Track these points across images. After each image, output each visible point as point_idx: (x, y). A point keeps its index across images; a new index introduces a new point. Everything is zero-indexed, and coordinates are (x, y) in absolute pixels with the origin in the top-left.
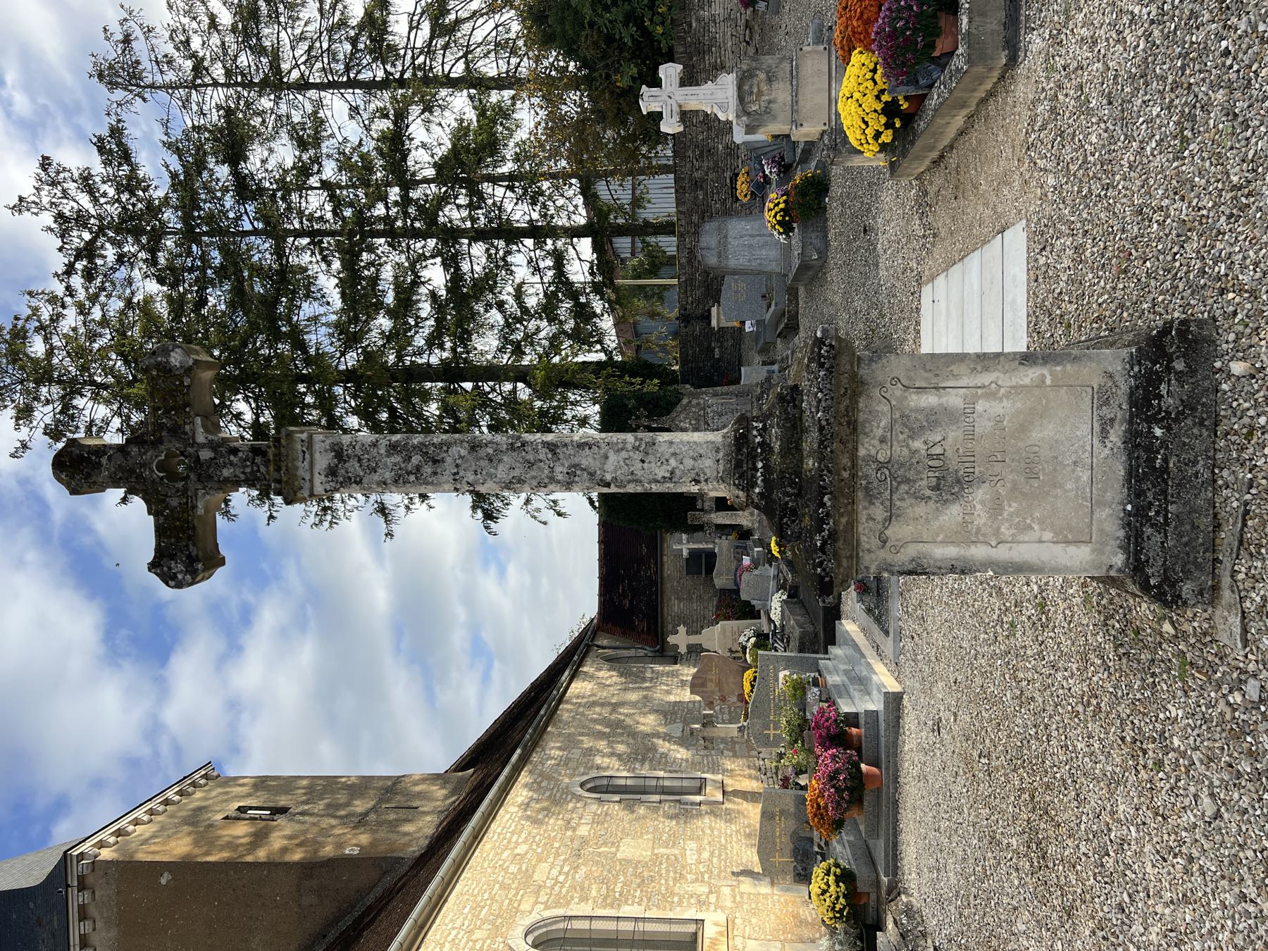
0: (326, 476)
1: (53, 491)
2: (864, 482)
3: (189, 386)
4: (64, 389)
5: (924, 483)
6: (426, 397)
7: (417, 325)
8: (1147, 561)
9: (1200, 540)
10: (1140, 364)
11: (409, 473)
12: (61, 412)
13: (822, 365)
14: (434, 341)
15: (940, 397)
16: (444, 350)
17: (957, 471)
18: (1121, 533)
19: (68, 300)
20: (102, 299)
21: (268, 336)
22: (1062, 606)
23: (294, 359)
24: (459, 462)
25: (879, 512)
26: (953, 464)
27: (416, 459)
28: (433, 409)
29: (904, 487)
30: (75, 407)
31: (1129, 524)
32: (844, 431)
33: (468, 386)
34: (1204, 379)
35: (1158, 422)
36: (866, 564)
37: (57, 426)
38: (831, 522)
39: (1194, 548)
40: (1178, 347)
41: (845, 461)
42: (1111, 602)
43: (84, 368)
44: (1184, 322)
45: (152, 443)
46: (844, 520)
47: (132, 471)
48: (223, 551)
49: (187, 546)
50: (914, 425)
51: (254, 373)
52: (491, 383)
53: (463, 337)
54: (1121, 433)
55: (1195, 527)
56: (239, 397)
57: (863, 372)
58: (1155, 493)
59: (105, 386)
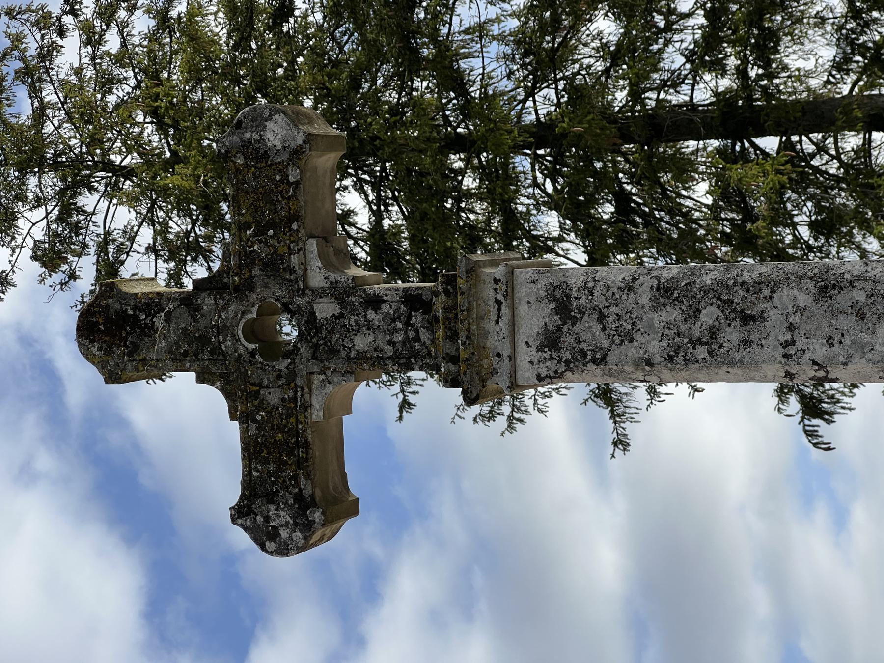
0: (540, 349)
1: (79, 374)
3: (297, 183)
4: (63, 179)
6: (684, 170)
7: (668, 28)
11: (695, 342)
12: (60, 219)
14: (704, 57)
16: (724, 73)
19: (68, 20)
20: (122, 14)
21: (397, 65)
23: (443, 108)
24: (795, 319)
27: (709, 315)
28: (701, 192)
30: (80, 210)
33: (770, 143)
37: (53, 245)
43: (94, 141)
45: (237, 289)
47: (203, 340)
48: (357, 483)
49: (295, 478)
51: (375, 138)
52: (817, 136)
53: (765, 47)
56: (348, 182)
59: (127, 173)
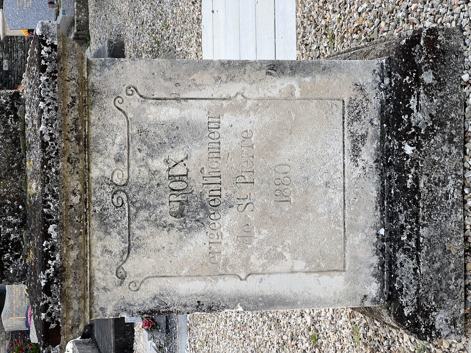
2: (98, 209)
5: (166, 208)
8: (401, 290)
9: (452, 266)
10: (390, 76)
13: (43, 69)
15: (181, 110)
17: (201, 194)
18: (375, 260)
22: (333, 338)
25: (115, 243)
26: (197, 186)
29: (143, 214)
31: (382, 250)
32: (73, 148)
34: (453, 93)
35: (408, 138)
36: (102, 305)
38: (58, 256)
39: (446, 274)
40: (427, 58)
41: (74, 183)
42: (376, 333)
44: (431, 31)
46: (74, 254)
50: (151, 141)
54: (373, 151)
55: (446, 252)
57: (94, 79)
58: (407, 216)
